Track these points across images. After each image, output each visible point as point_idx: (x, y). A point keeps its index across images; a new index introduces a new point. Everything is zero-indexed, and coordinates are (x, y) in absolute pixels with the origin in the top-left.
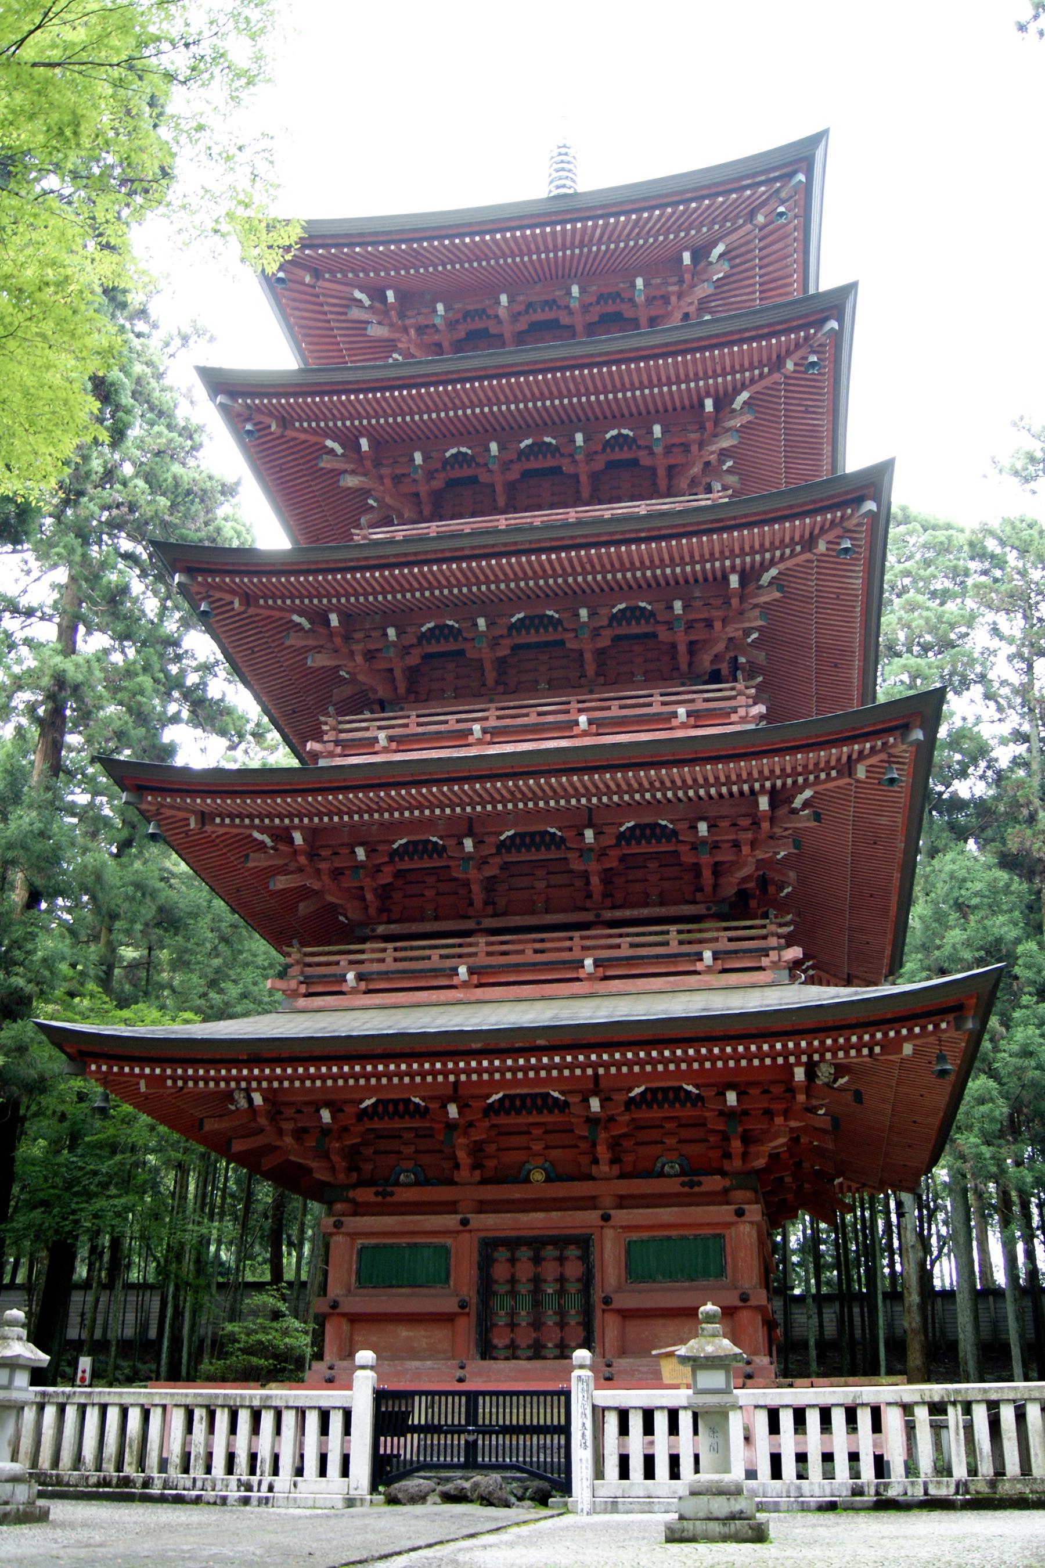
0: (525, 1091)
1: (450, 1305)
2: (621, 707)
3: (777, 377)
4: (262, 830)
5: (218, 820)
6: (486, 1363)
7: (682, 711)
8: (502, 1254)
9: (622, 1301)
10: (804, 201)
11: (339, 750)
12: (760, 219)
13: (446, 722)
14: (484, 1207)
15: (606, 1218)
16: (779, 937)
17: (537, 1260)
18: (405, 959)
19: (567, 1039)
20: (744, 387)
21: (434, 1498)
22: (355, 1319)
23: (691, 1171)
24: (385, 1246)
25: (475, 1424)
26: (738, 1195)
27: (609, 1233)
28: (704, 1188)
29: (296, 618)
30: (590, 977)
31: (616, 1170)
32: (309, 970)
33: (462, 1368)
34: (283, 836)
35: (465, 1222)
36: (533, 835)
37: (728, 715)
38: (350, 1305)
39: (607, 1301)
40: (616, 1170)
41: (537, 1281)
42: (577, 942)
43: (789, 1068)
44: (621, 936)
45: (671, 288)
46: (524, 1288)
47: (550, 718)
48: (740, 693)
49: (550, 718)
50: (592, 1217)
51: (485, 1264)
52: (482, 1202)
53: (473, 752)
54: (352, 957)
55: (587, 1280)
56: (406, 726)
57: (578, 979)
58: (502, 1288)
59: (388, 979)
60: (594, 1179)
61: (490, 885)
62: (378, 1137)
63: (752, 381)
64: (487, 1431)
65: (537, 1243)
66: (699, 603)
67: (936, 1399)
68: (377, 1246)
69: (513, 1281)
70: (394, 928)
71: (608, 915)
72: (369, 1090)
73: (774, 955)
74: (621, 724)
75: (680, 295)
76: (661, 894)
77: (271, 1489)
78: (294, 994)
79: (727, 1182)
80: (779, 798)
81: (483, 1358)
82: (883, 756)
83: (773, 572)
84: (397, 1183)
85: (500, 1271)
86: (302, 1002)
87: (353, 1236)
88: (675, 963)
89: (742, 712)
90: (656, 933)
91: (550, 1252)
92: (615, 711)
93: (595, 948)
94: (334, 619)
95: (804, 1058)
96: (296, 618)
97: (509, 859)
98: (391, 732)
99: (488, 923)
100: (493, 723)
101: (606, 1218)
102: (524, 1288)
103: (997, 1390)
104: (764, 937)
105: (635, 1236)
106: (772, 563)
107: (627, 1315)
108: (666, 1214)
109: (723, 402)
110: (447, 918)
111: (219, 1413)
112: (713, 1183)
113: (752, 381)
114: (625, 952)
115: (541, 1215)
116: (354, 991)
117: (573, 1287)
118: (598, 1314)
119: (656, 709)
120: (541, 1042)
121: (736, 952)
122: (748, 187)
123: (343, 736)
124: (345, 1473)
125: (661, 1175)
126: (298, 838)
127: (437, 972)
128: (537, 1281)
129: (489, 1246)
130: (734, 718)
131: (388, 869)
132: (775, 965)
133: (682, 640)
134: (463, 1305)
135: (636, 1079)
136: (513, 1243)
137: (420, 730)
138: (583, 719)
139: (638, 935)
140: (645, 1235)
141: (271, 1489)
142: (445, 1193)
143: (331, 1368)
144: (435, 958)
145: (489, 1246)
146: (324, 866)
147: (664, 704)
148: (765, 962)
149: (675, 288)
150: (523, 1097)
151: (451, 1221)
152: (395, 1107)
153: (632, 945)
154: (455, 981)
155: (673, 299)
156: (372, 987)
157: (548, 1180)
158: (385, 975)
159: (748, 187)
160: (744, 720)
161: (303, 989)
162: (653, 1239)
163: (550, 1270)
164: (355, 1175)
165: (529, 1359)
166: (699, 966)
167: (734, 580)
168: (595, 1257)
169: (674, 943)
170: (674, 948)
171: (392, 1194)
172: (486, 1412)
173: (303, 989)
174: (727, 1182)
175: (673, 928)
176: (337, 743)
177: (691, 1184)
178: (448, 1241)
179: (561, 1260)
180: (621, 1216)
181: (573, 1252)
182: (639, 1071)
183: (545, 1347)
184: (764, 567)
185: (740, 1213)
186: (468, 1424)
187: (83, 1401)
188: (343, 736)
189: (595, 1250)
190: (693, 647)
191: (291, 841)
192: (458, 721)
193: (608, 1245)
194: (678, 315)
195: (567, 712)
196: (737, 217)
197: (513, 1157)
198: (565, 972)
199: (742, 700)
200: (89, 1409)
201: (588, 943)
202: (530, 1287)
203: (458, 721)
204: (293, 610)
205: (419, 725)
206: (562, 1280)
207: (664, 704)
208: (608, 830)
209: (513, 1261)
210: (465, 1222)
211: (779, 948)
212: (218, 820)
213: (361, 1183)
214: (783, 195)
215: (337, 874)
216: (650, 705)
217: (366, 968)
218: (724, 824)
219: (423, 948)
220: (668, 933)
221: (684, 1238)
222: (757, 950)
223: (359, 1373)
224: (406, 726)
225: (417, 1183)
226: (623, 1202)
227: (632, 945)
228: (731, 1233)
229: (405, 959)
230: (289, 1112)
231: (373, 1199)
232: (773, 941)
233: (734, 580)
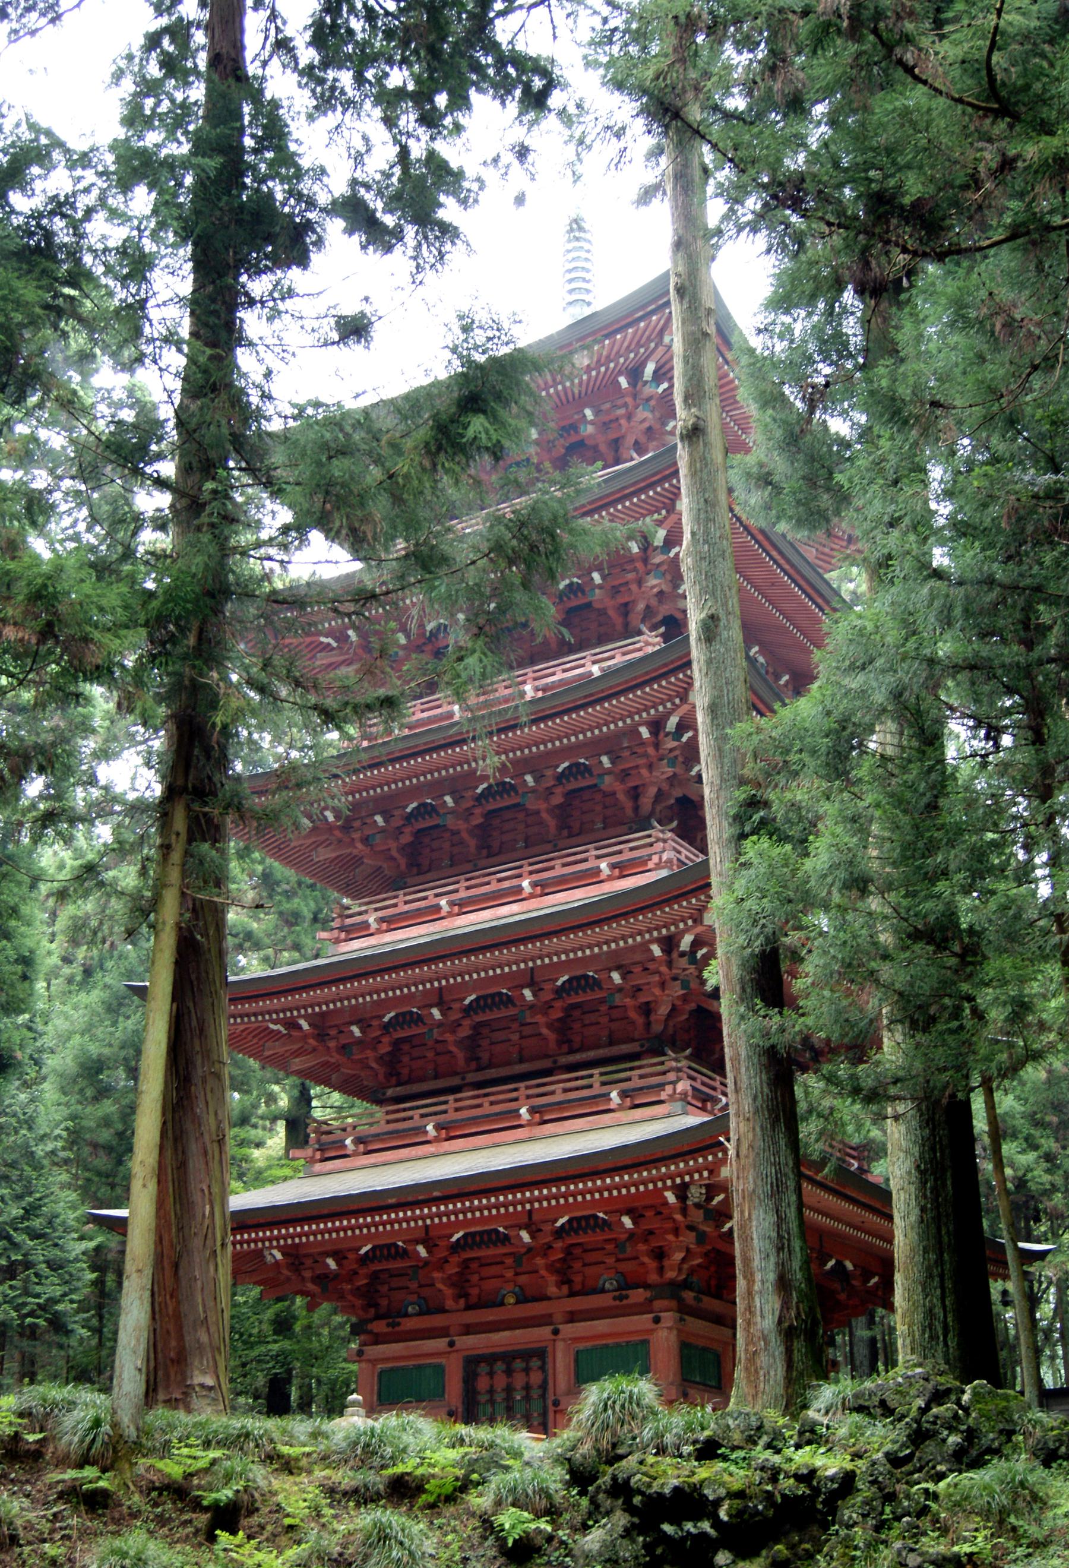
0: (478, 1229)
4: (275, 1022)
8: (483, 1368)
13: (425, 898)
14: (468, 1330)
17: (509, 1372)
18: (397, 1121)
19: (510, 1181)
23: (627, 1284)
24: (398, 1369)
26: (658, 1304)
27: (560, 1345)
28: (631, 1301)
30: (530, 1124)
31: (565, 1289)
34: (292, 1025)
35: (451, 1344)
36: (493, 996)
37: (645, 863)
40: (565, 1289)
41: (509, 1390)
42: (596, 1080)
43: (659, 1192)
44: (631, 1069)
46: (499, 1397)
50: (546, 1331)
51: (469, 1379)
52: (572, 1313)
53: (284, 970)
54: (492, 1098)
55: (544, 1386)
56: (395, 905)
58: (483, 1398)
59: (383, 1141)
60: (549, 1299)
61: (472, 1044)
62: (585, 1251)
65: (508, 1358)
66: (626, 753)
68: (392, 1369)
69: (491, 1391)
70: (400, 1090)
71: (564, 1060)
72: (458, 1225)
73: (669, 1089)
74: (563, 883)
76: (610, 1036)
78: (311, 1161)
79: (648, 1294)
84: (406, 1315)
85: (483, 1384)
86: (318, 1167)
87: (373, 1362)
91: (518, 1364)
92: (559, 871)
93: (435, 1114)
97: (397, 1036)
98: (380, 914)
99: (471, 1077)
101: (556, 1332)
102: (499, 1397)
104: (664, 1073)
105: (581, 1346)
108: (601, 1326)
110: (444, 1076)
112: (638, 1295)
114: (559, 1097)
115: (507, 1333)
116: (355, 1154)
117: (535, 1393)
118: (551, 1415)
120: (436, 1194)
122: (641, 319)
123: (348, 921)
125: (603, 1291)
126: (304, 1025)
128: (509, 1390)
129: (472, 1364)
131: (386, 1040)
132: (672, 1098)
133: (620, 790)
135: (560, 1211)
136: (491, 1359)
137: (407, 908)
140: (589, 1344)
142: (437, 1321)
145: (472, 1364)
146: (332, 1044)
148: (663, 1096)
150: (481, 1233)
151: (441, 1344)
152: (386, 1251)
153: (641, 1077)
157: (518, 1302)
158: (377, 1137)
159: (641, 319)
160: (658, 866)
161: (318, 1155)
162: (595, 1348)
163: (519, 1380)
164: (462, 1301)
168: (549, 1366)
169: (597, 1085)
171: (627, 1297)
174: (648, 1294)
175: (596, 1071)
176: (341, 929)
177: (621, 1298)
178: (443, 1361)
179: (527, 1370)
180: (568, 1330)
181: (535, 1363)
182: (558, 1205)
184: (668, 715)
185: (657, 1320)
188: (348, 921)
189: (549, 1360)
190: (635, 793)
191: (300, 1027)
193: (559, 1355)
197: (490, 1285)
198: (507, 1122)
202: (503, 1395)
206: (527, 1388)
208: (547, 986)
209: (491, 1374)
210: (451, 1344)
213: (378, 1317)
215: (343, 1048)
216: (586, 860)
218: (637, 969)
221: (618, 1345)
224: (395, 905)
225: (420, 1314)
226: (572, 1317)
227: (641, 1077)
228: (653, 1338)
229: (397, 1121)
230: (309, 1262)
231: (386, 1330)
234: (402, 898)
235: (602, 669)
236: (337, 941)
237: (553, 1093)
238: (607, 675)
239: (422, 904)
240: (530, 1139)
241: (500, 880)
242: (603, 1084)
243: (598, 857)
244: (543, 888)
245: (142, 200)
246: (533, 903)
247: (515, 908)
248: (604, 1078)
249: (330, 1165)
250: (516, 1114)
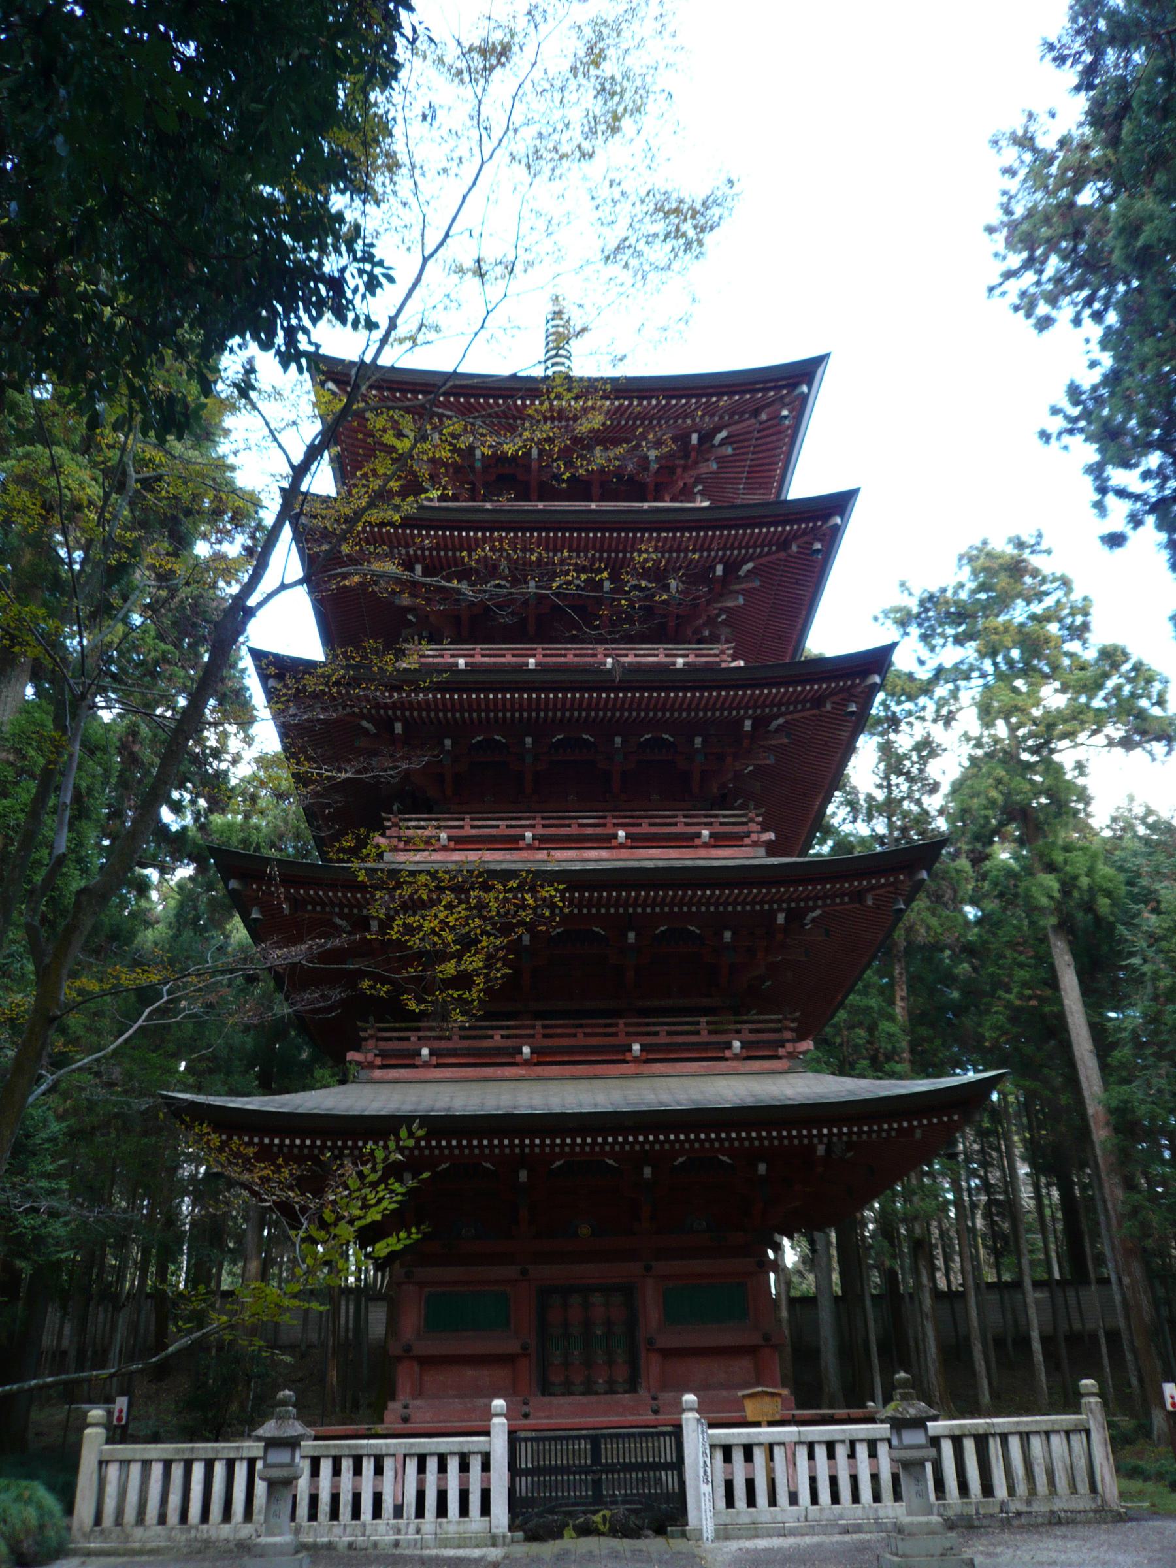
1: (511, 1346)
2: (651, 825)
3: (782, 555)
4: (341, 916)
5: (309, 907)
6: (547, 1399)
7: (705, 833)
9: (663, 1342)
10: (801, 406)
11: (402, 845)
12: (764, 417)
13: (497, 827)
15: (648, 1268)
16: (792, 1030)
20: (751, 559)
21: (569, 1532)
22: (428, 1362)
25: (600, 1464)
29: (364, 723)
32: (382, 1044)
33: (526, 1404)
35: (524, 1272)
37: (742, 838)
38: (420, 1349)
39: (650, 1342)
45: (677, 462)
47: (590, 831)
48: (751, 820)
49: (590, 831)
56: (461, 827)
57: (624, 1061)
63: (760, 555)
64: (611, 1469)
67: (981, 1431)
73: (789, 1047)
75: (685, 468)
77: (418, 1531)
80: (795, 916)
81: (543, 1395)
82: (891, 889)
83: (781, 721)
86: (378, 1073)
88: (706, 1050)
89: (754, 837)
90: (687, 1023)
94: (398, 728)
95: (825, 1140)
96: (364, 723)
100: (540, 831)
103: (1027, 1423)
106: (782, 715)
107: (666, 1353)
109: (732, 567)
111: (365, 1461)
113: (760, 555)
116: (426, 1065)
119: (680, 829)
121: (758, 1042)
124: (485, 1510)
127: (499, 1051)
130: (747, 841)
134: (524, 1348)
137: (474, 832)
138: (621, 833)
139: (674, 1024)
141: (418, 1531)
143: (406, 1407)
144: (497, 1038)
147: (687, 824)
148: (781, 1052)
149: (682, 462)
154: (518, 1059)
155: (679, 471)
156: (441, 1061)
158: (453, 1053)
165: (583, 1394)
166: (728, 1054)
167: (748, 725)
169: (455, 1037)
170: (704, 1037)
172: (610, 1453)
173: (378, 1061)
176: (400, 839)
183: (596, 1383)
186: (593, 1464)
187: (232, 1455)
192: (508, 826)
194: (681, 484)
195: (604, 825)
196: (744, 412)
199: (753, 827)
200: (237, 1464)
201: (632, 1030)
203: (508, 826)
204: (362, 716)
205: (473, 827)
207: (687, 824)
210: (524, 1272)
211: (794, 1041)
212: (309, 907)
214: (787, 400)
216: (675, 824)
217: (438, 1044)
219: (487, 1028)
220: (698, 1023)
222: (775, 1042)
223: (496, 1420)
224: (461, 827)
227: (669, 1033)
232: (788, 1035)
233: (748, 725)
234: (467, 822)
235: (466, 664)
236: (395, 849)
237: (656, 1034)
238: (472, 669)
239: (494, 832)
240: (637, 1076)
241: (580, 825)
242: (628, 1034)
243: (615, 825)
244: (636, 841)
245: (1080, 40)
246: (624, 853)
247: (604, 854)
248: (712, 1027)
249: (756, 1065)
250: (729, 1046)
